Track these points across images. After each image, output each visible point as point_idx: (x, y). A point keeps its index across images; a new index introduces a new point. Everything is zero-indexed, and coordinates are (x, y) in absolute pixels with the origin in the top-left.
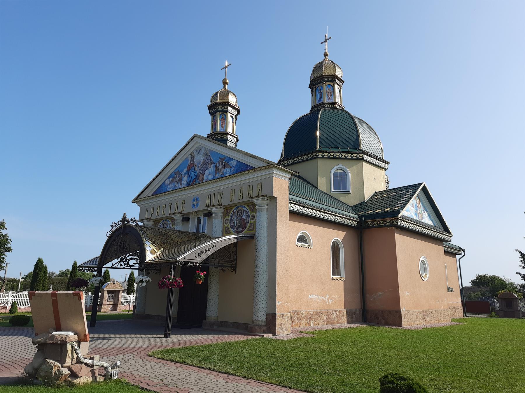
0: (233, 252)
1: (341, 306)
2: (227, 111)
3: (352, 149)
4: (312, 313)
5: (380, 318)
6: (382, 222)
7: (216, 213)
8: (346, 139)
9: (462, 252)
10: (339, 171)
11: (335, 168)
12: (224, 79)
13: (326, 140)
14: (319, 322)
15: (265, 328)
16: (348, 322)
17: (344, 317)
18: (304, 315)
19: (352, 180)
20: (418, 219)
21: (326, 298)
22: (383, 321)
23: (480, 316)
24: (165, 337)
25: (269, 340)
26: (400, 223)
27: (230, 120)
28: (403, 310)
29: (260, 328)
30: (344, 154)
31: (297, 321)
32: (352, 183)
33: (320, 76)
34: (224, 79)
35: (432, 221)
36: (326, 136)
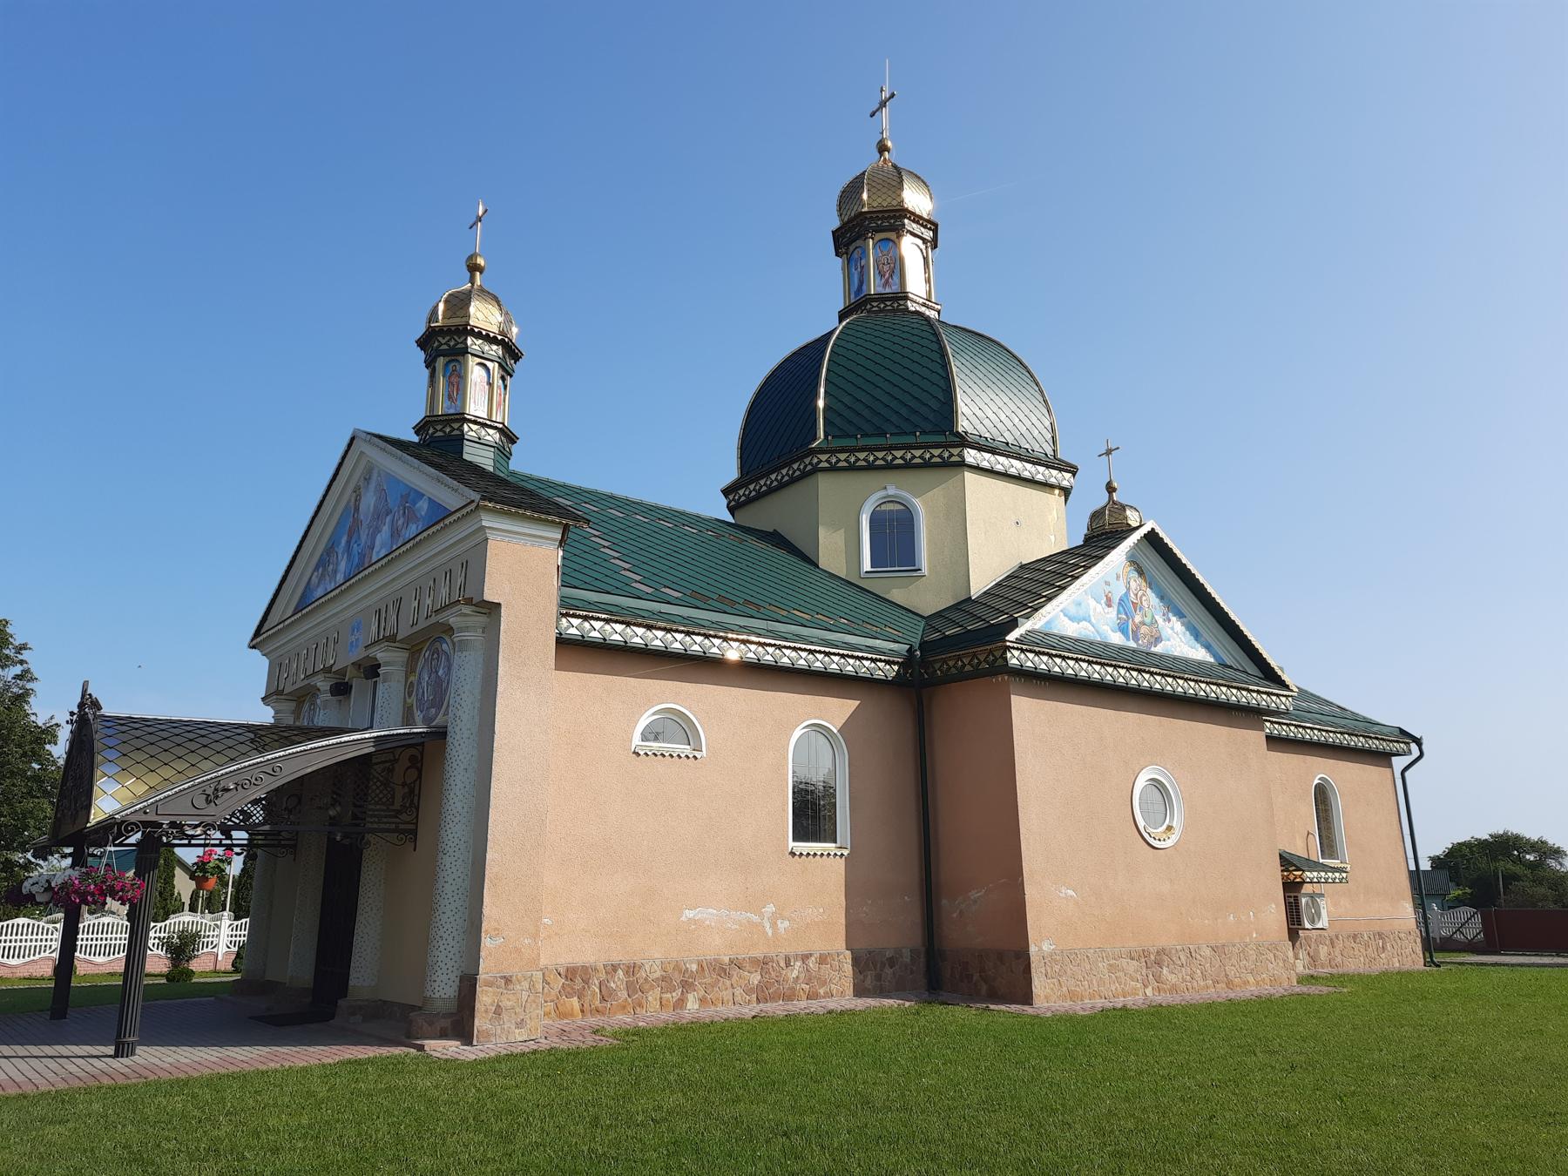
1: (837, 943)
2: (465, 351)
4: (694, 967)
6: (966, 661)
7: (387, 664)
8: (912, 403)
9: (1414, 746)
10: (891, 507)
11: (871, 496)
12: (472, 257)
13: (847, 413)
14: (727, 995)
15: (446, 1023)
16: (859, 992)
17: (843, 974)
18: (658, 974)
19: (930, 532)
20: (1132, 644)
21: (762, 915)
22: (984, 988)
23: (1546, 960)
26: (1014, 659)
27: (476, 374)
29: (431, 1024)
33: (856, 216)
34: (472, 257)
35: (1208, 647)
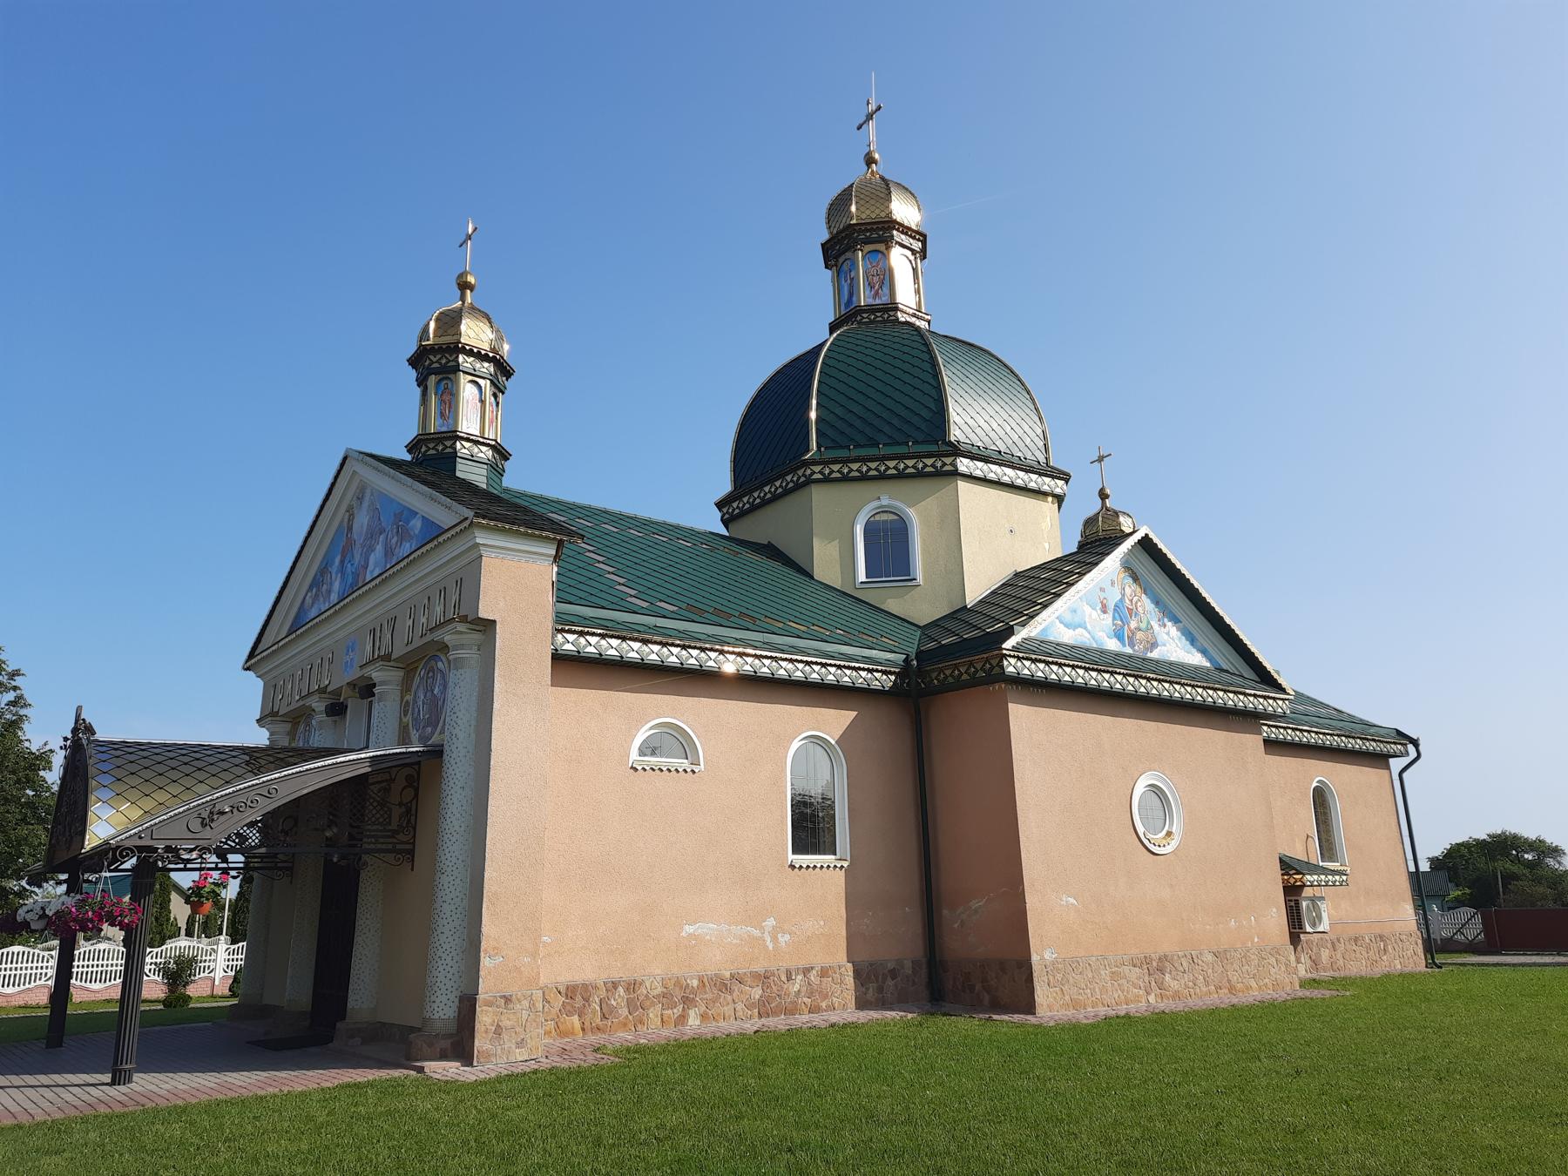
0: (400, 804)
1: (837, 956)
2: (456, 369)
3: (923, 442)
4: (695, 983)
5: (978, 987)
7: (383, 683)
8: (904, 413)
9: (1411, 748)
10: (884, 517)
12: (462, 275)
14: (728, 1010)
15: (446, 1044)
16: (862, 1004)
18: (659, 990)
19: (924, 541)
20: (1128, 650)
21: (762, 929)
22: (986, 998)
24: (113, 1083)
25: (449, 1086)
26: (1011, 666)
28: (1042, 954)
30: (891, 464)
31: (624, 1012)
32: (925, 551)
34: (462, 275)
35: (1204, 652)
36: (839, 411)
